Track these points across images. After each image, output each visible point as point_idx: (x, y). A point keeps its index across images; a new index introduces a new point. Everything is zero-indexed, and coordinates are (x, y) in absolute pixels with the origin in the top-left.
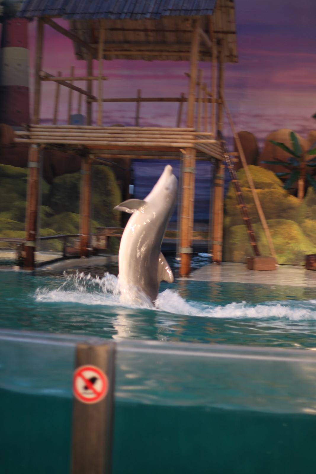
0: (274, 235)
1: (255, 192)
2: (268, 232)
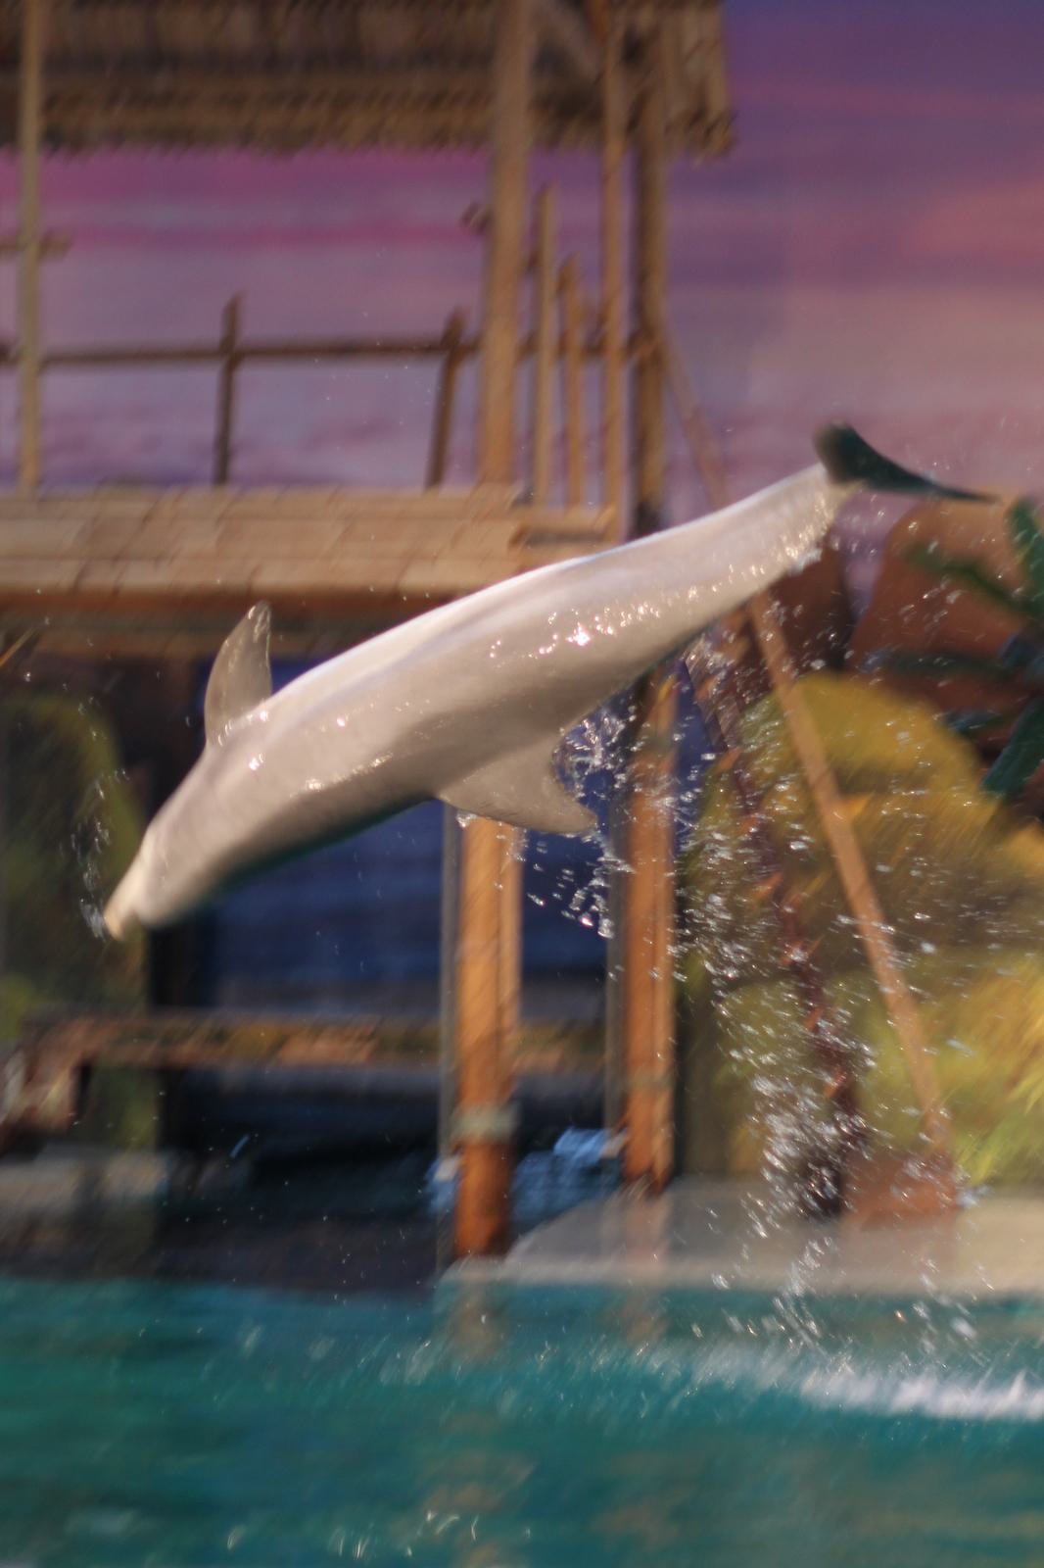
0: (942, 1033)
1: (840, 817)
2: (905, 1024)
